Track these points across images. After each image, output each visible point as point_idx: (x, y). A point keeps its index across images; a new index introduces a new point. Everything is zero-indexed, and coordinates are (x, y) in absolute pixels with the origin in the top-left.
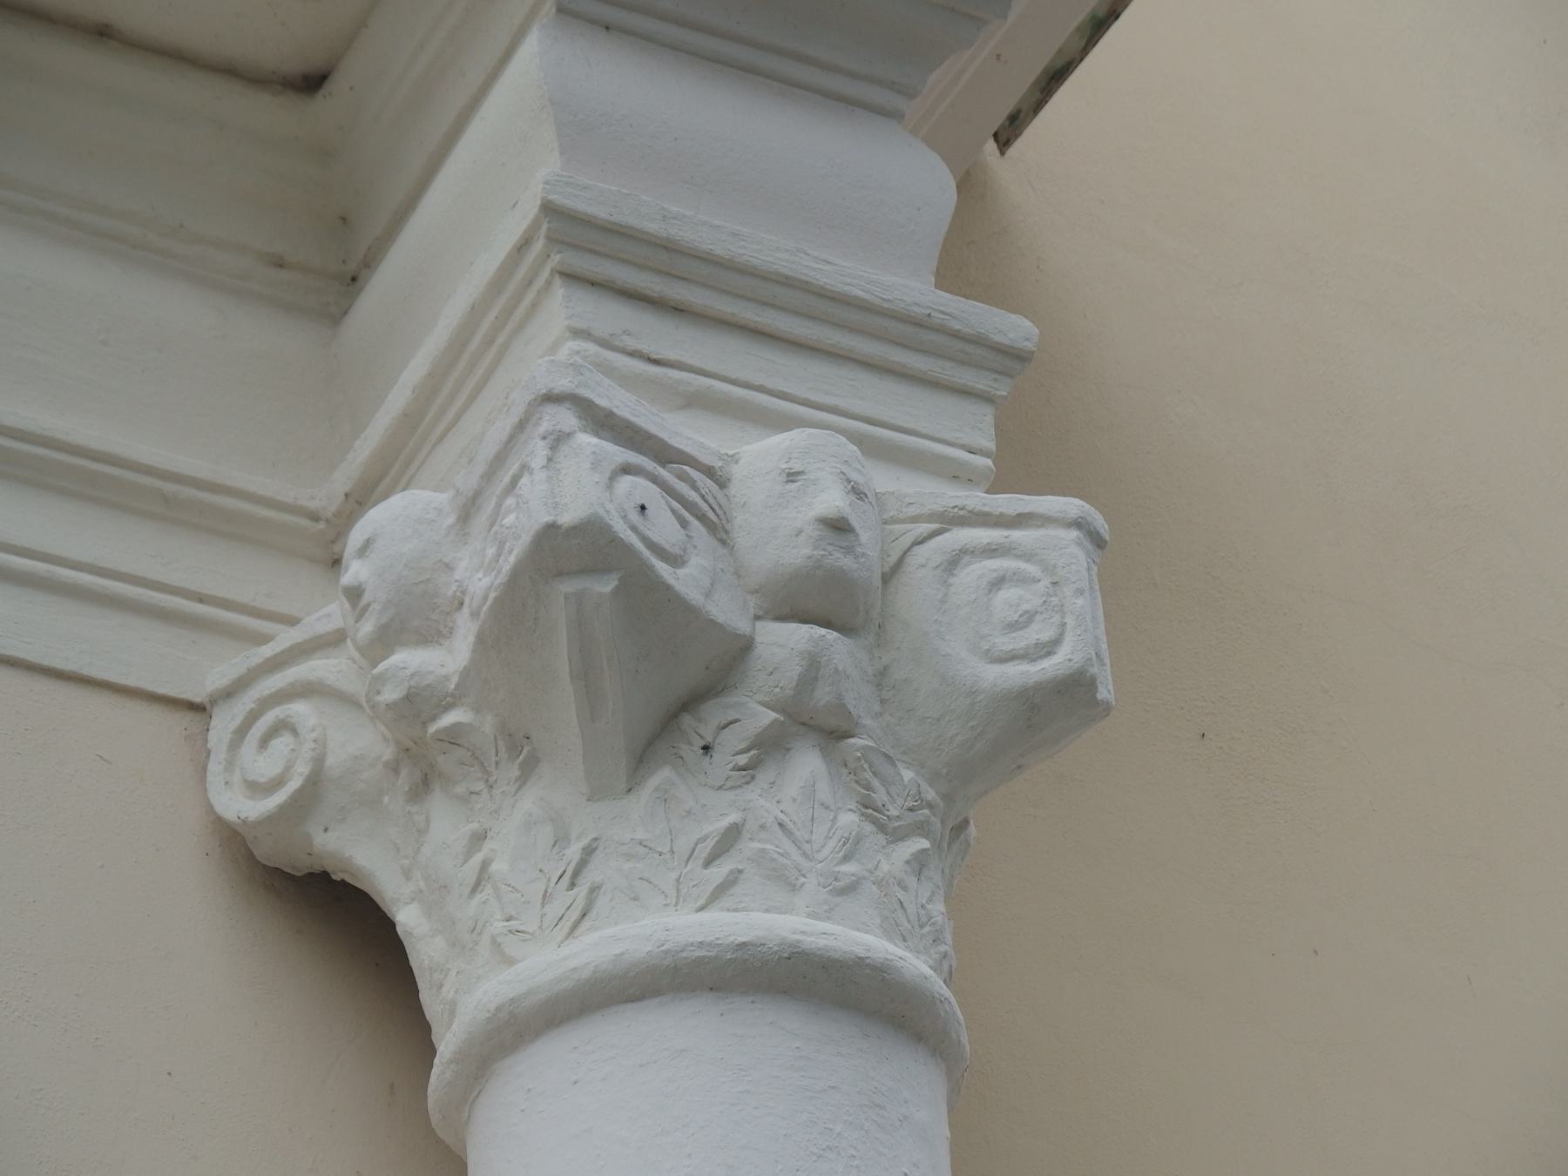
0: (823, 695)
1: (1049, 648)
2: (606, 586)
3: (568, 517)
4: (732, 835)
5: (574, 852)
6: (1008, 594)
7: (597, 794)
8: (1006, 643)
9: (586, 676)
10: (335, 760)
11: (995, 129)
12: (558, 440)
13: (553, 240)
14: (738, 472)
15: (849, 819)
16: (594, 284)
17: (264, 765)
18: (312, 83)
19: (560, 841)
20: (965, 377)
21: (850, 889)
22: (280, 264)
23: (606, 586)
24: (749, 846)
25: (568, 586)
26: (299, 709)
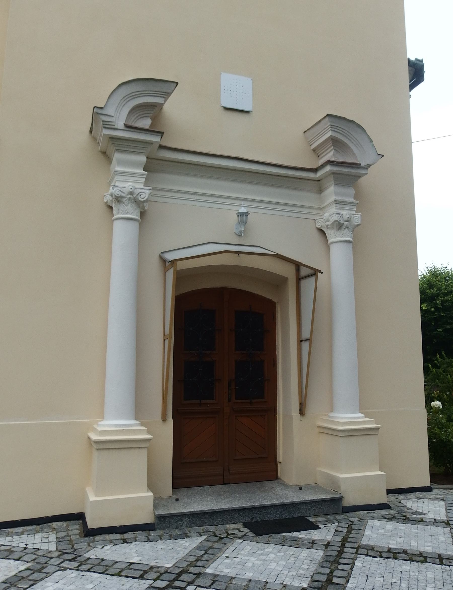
0: (347, 226)
1: (358, 222)
2: (338, 223)
3: (336, 220)
4: (343, 234)
5: (335, 234)
6: (356, 219)
7: (336, 231)
8: (356, 222)
9: (336, 226)
10: (323, 225)
11: (329, 114)
12: (335, 215)
13: (335, 202)
14: (344, 214)
15: (348, 232)
16: (337, 204)
17: (319, 224)
18: (319, 181)
19: (335, 233)
20: (355, 205)
21: (348, 236)
22: (317, 190)
23: (338, 223)
24: (344, 234)
25: (336, 223)
26: (320, 222)
